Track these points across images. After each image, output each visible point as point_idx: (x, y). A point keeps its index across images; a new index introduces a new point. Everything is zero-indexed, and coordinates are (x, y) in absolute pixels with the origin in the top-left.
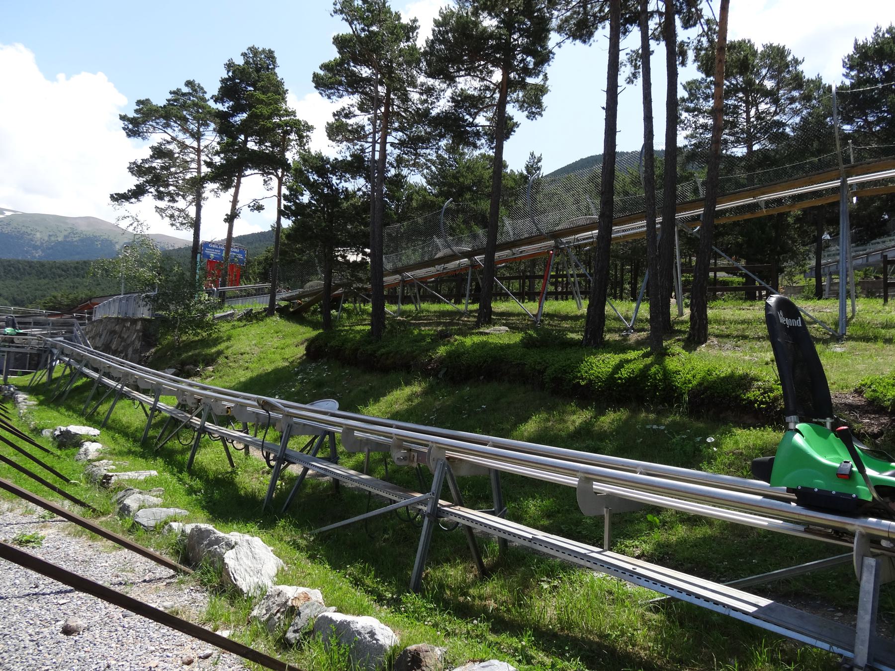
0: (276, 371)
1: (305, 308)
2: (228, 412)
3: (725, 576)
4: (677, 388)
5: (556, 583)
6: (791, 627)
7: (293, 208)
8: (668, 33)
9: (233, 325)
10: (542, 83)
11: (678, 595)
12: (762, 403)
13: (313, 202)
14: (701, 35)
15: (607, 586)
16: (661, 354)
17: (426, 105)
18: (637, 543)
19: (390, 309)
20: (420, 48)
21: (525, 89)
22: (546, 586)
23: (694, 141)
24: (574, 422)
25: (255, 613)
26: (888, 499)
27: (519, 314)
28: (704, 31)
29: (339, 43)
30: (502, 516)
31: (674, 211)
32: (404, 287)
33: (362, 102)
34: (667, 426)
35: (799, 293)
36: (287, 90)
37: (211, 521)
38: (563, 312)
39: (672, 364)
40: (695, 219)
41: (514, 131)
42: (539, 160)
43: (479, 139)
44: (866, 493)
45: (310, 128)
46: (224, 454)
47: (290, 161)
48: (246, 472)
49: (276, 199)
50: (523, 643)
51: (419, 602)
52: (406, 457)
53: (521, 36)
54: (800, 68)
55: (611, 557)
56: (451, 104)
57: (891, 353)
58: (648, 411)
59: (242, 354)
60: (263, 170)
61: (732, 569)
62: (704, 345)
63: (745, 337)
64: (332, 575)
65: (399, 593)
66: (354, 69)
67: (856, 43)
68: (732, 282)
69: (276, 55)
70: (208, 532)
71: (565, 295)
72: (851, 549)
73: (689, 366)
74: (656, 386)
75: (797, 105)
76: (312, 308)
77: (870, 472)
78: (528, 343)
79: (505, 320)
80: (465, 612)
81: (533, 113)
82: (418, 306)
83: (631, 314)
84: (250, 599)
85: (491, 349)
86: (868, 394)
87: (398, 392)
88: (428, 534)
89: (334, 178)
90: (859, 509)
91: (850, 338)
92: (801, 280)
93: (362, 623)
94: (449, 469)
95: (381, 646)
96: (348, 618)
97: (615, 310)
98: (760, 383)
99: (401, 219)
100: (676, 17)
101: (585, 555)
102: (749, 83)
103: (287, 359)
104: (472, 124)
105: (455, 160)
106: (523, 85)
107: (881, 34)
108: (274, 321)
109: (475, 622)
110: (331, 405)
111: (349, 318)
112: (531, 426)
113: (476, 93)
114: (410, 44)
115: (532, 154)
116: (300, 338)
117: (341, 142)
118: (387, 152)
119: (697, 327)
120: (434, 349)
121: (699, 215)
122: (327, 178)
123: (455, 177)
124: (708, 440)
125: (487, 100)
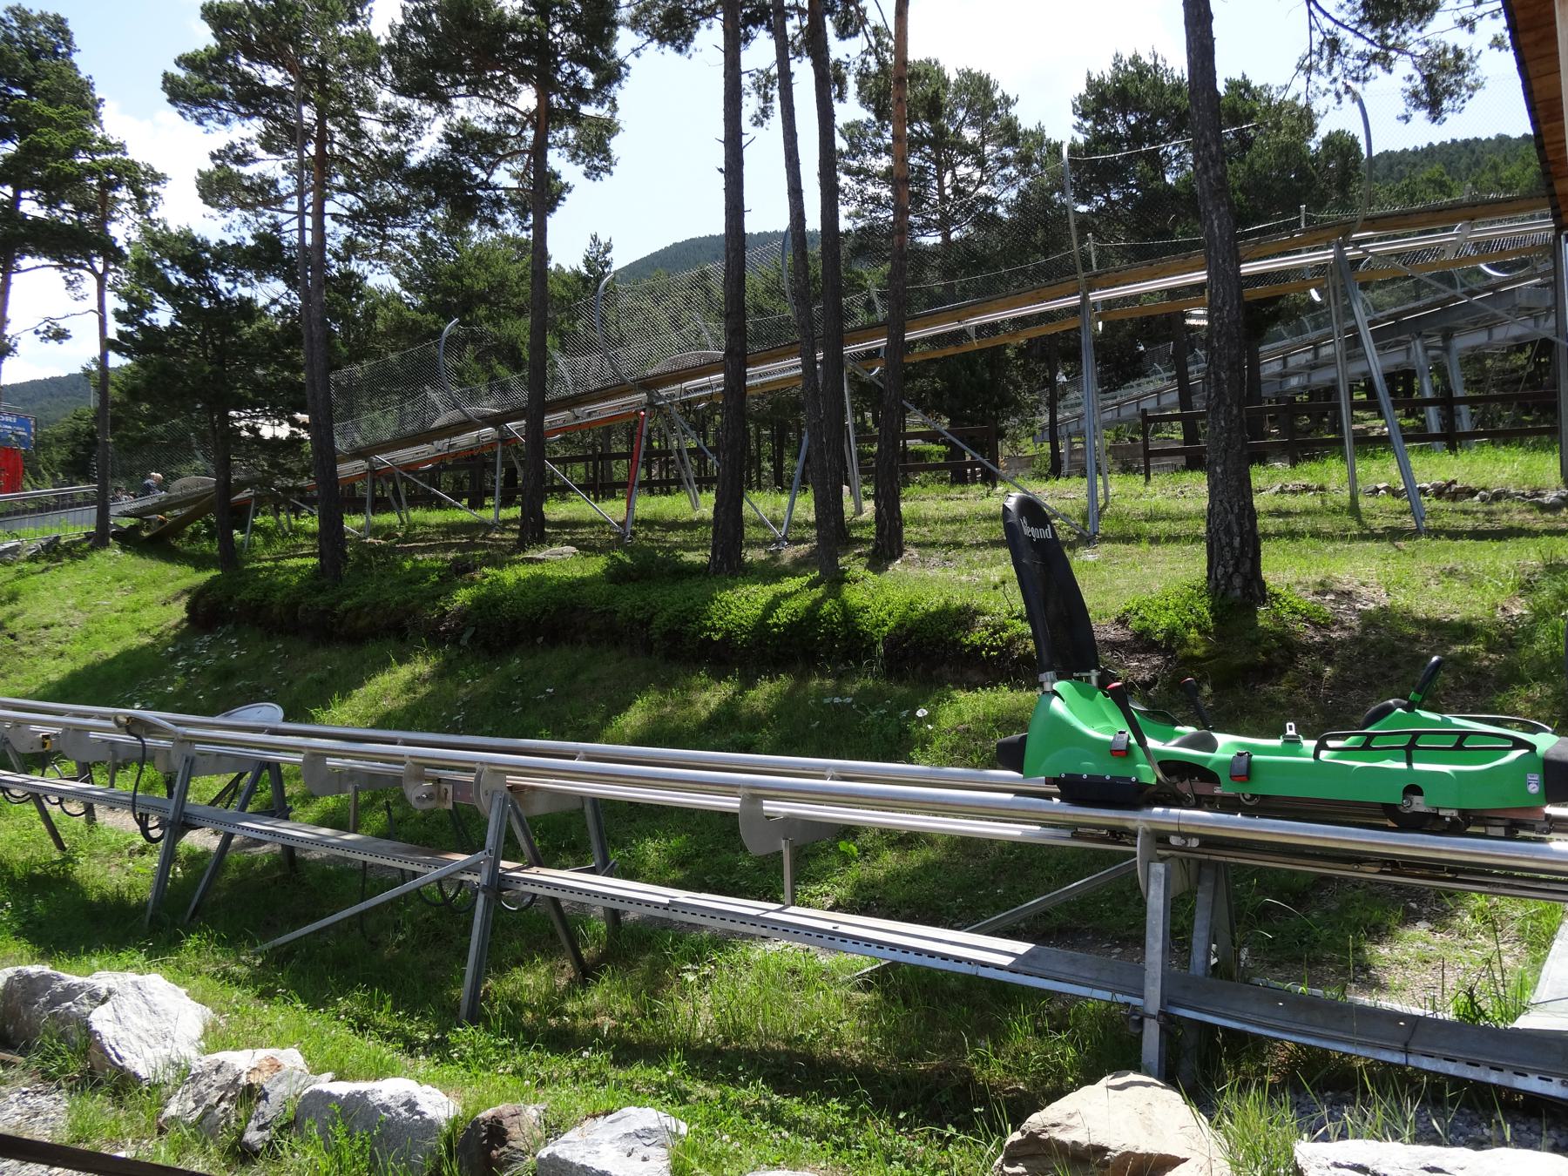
0: (128, 656)
1: (177, 528)
2: (44, 745)
3: (959, 921)
4: (866, 634)
5: (707, 970)
6: (1063, 977)
7: (139, 336)
8: (815, 45)
9: (19, 571)
10: (608, 115)
11: (898, 956)
12: (992, 648)
13: (179, 324)
14: (866, 52)
15: (788, 962)
16: (836, 580)
17: (396, 145)
18: (826, 888)
19: (353, 523)
20: (379, 39)
21: (580, 125)
22: (691, 978)
23: (861, 223)
24: (707, 703)
25: (172, 1110)
26: (1175, 779)
27: (592, 523)
28: (870, 46)
29: (215, 18)
30: (610, 874)
31: (841, 344)
32: (374, 481)
33: (268, 133)
34: (854, 696)
35: (1028, 466)
36: (101, 100)
37: (46, 955)
38: (669, 517)
39: (855, 595)
40: (871, 355)
41: (564, 199)
42: (608, 249)
43: (501, 213)
44: (1148, 774)
45: (158, 179)
46: (41, 826)
47: (121, 243)
48: (93, 855)
49: (96, 317)
50: (670, 1073)
51: (482, 1038)
52: (431, 794)
53: (567, 29)
54: (1013, 111)
55: (796, 915)
56: (444, 146)
57: (1159, 559)
58: (823, 675)
59: (46, 627)
60: (61, 259)
61: (970, 907)
62: (899, 562)
63: (958, 545)
64: (313, 1020)
65: (443, 1029)
66: (247, 69)
67: (1089, 79)
68: (930, 454)
69: (71, 26)
70: (46, 980)
71: (665, 487)
72: (1134, 855)
73: (882, 598)
74: (833, 633)
75: (1011, 171)
76: (189, 529)
77: (1152, 744)
78: (617, 575)
79: (569, 534)
80: (563, 1041)
81: (596, 168)
82: (404, 515)
83: (781, 514)
84: (155, 1086)
85: (554, 589)
86: (1134, 624)
87: (387, 677)
88: (485, 921)
89: (222, 278)
90: (1133, 796)
91: (1105, 539)
92: (1029, 447)
93: (389, 1090)
94: (514, 807)
95: (431, 1122)
96: (362, 1086)
97: (756, 510)
98: (987, 618)
99: (356, 357)
100: (827, 18)
101: (757, 917)
102: (941, 132)
103: (148, 631)
104: (486, 185)
105: (453, 245)
106: (575, 119)
107: (1122, 66)
108: (110, 558)
109: (585, 1054)
110: (270, 713)
111: (268, 544)
112: (635, 717)
113: (490, 128)
114: (359, 29)
115: (595, 238)
116: (170, 589)
117: (230, 208)
118: (327, 231)
119: (886, 532)
120: (448, 594)
121: (878, 350)
122: (207, 278)
123: (454, 276)
124: (919, 714)
125: (512, 141)
